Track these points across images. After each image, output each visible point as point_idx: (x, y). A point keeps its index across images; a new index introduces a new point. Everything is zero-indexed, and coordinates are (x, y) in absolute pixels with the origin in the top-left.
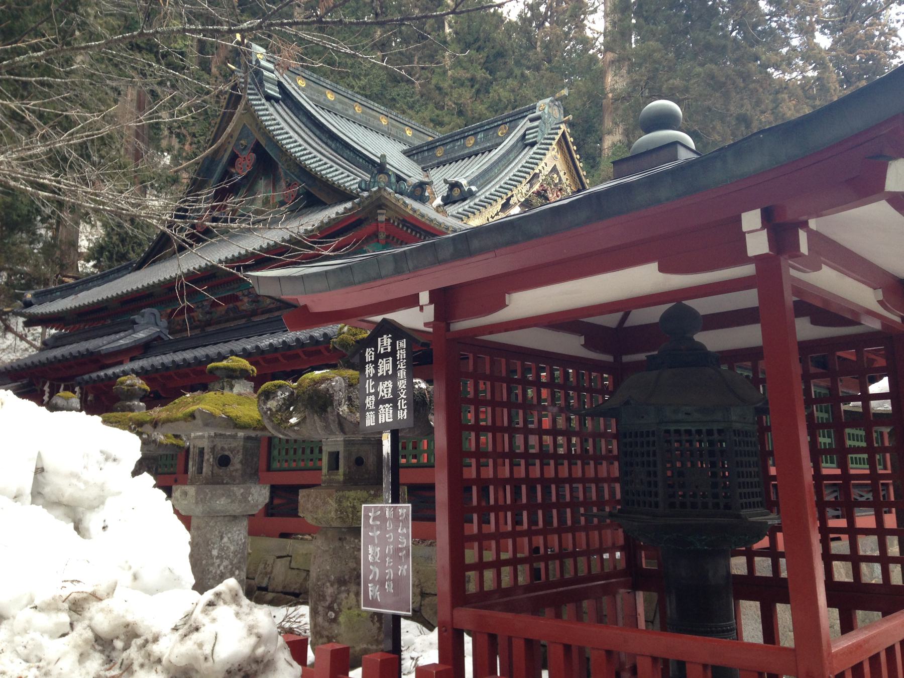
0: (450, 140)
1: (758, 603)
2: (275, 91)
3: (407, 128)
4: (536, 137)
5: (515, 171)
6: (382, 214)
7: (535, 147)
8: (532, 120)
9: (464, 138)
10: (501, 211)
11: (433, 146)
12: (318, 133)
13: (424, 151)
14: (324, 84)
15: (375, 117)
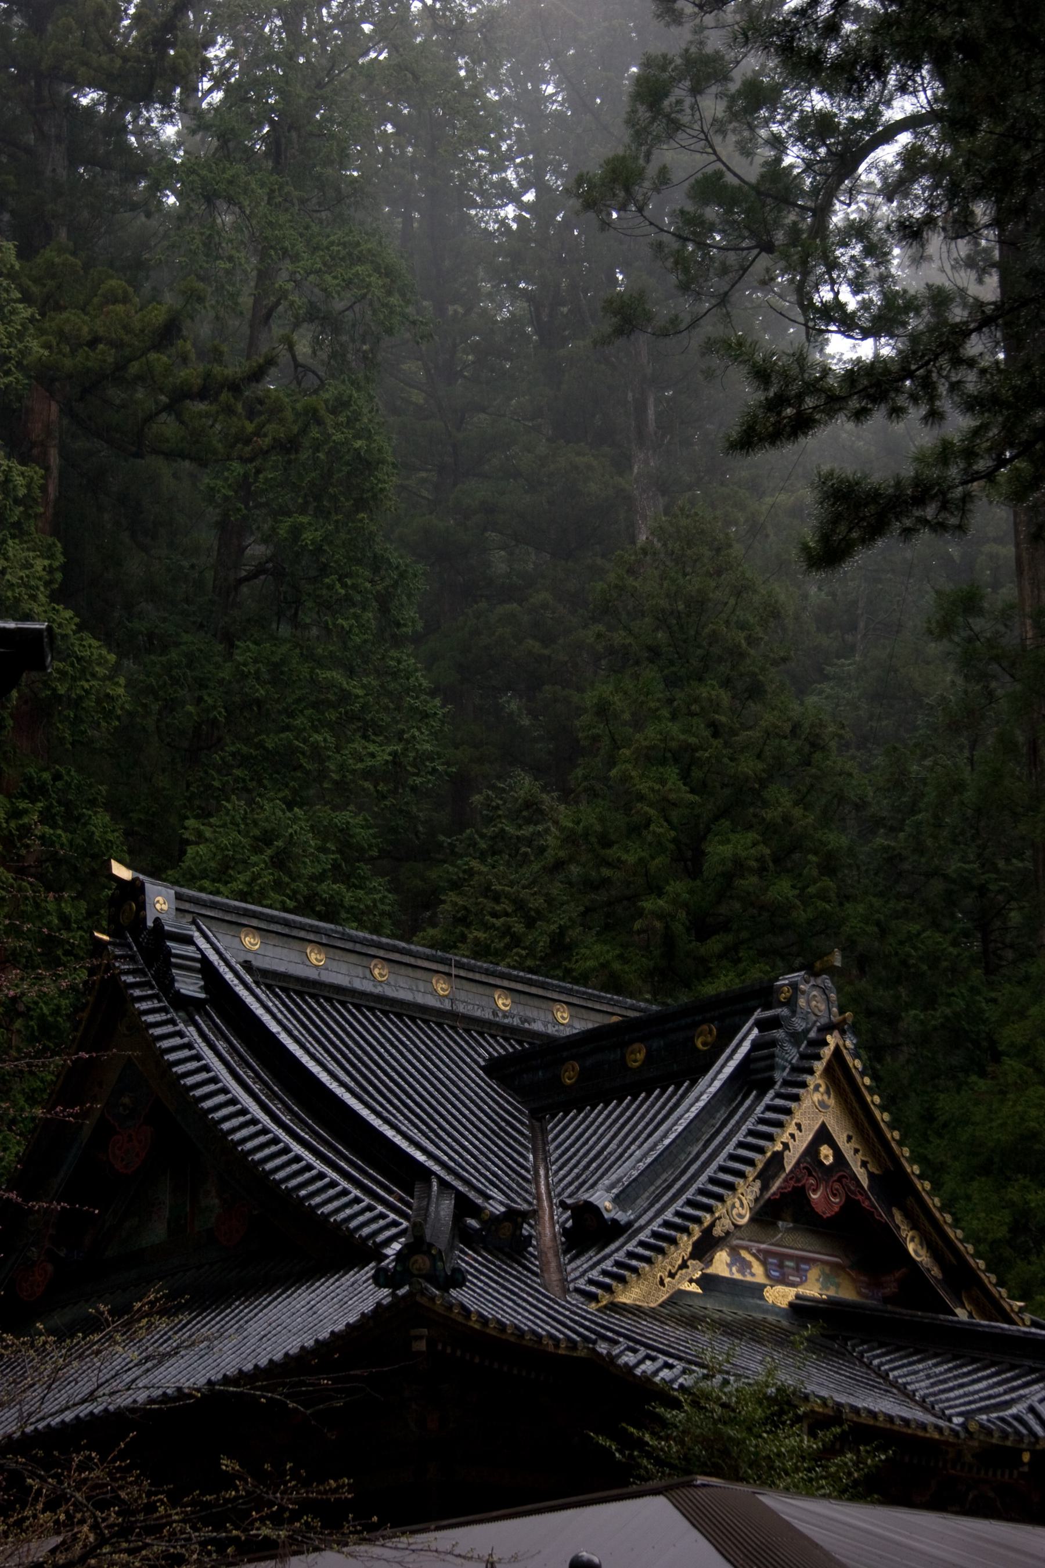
5: (702, 1181)
10: (693, 1256)
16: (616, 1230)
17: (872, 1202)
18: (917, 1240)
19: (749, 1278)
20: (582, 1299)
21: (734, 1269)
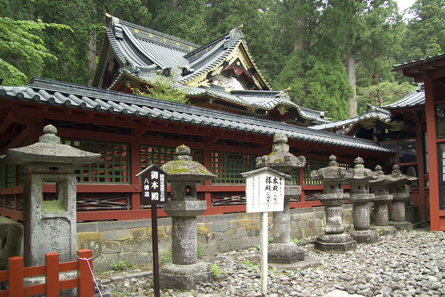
2: (121, 36)
4: (227, 46)
6: (128, 83)
7: (227, 50)
8: (227, 39)
9: (205, 48)
12: (135, 51)
14: (148, 31)
15: (173, 43)
16: (190, 73)
17: (248, 73)
19: (222, 86)
20: (251, 121)
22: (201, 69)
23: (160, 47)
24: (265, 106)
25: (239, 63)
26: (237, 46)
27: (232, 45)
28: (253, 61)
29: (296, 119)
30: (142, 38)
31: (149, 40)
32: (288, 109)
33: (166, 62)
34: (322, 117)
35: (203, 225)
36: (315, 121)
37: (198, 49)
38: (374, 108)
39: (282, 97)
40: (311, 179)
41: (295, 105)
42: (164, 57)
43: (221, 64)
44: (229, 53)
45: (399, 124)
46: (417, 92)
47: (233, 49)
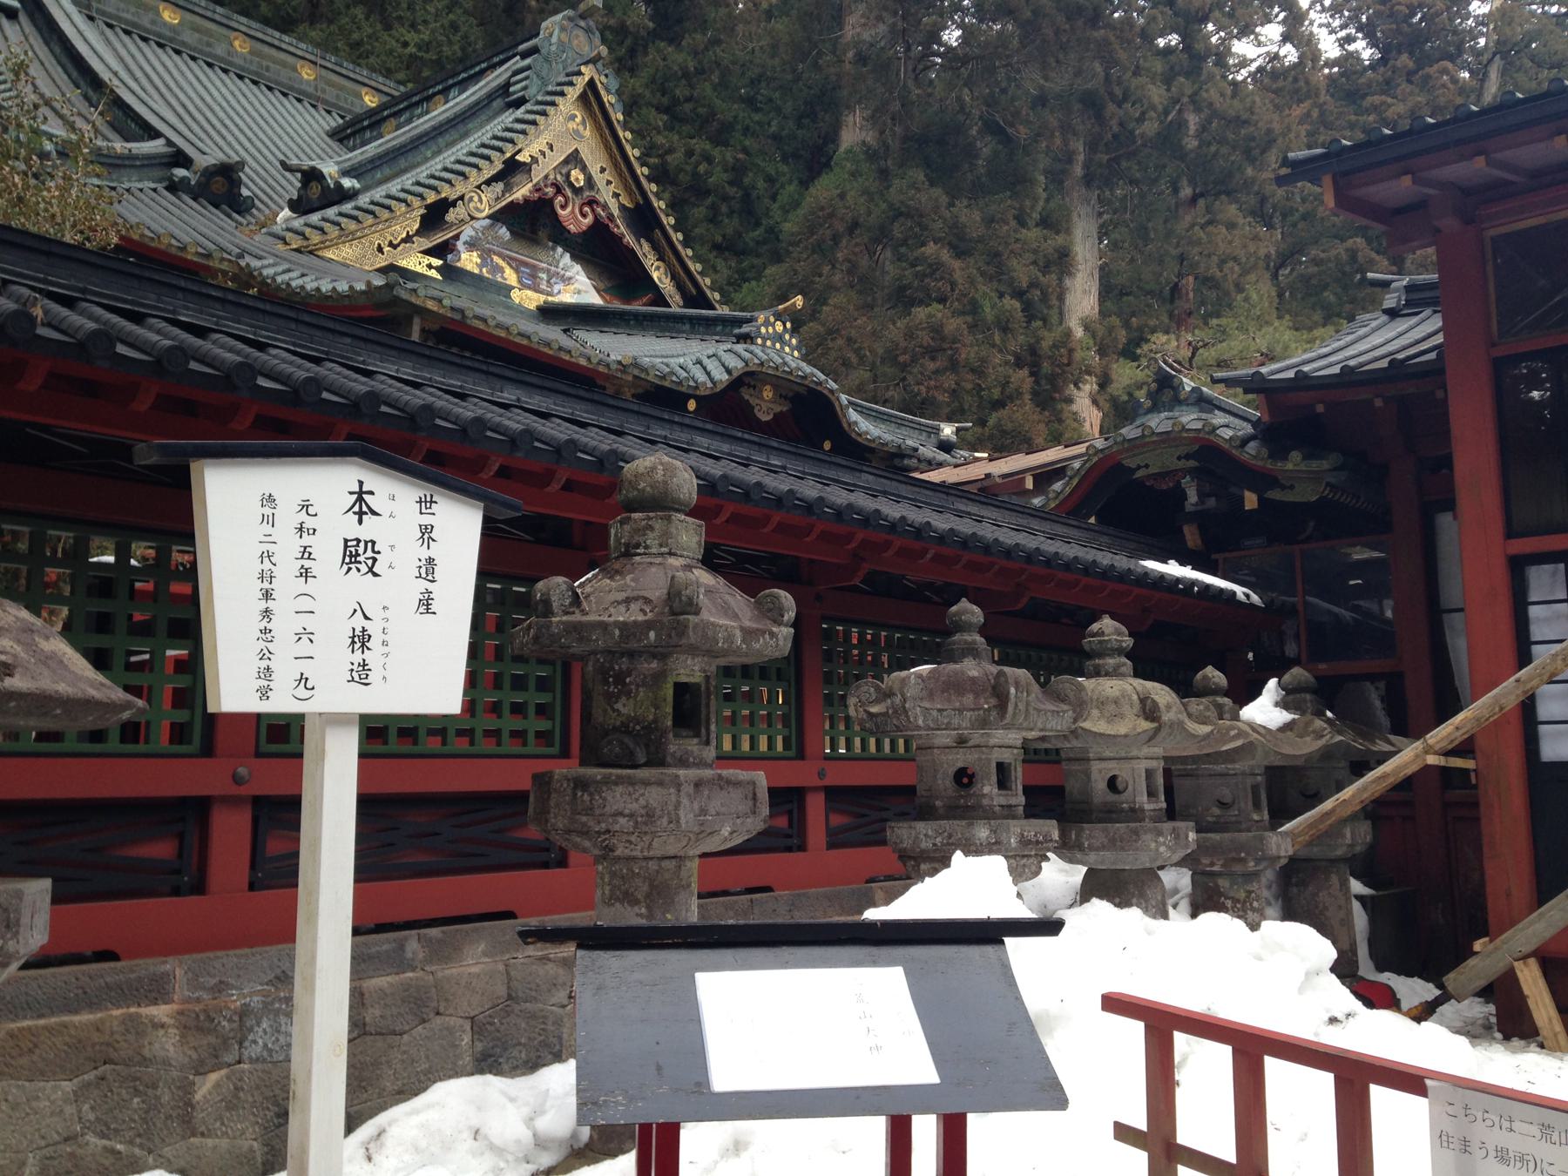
0: (405, 104)
1: (1331, 1076)
3: (364, 90)
4: (525, 88)
7: (522, 109)
8: (524, 55)
11: (378, 117)
12: (75, 74)
13: (364, 129)
15: (284, 64)
16: (344, 196)
18: (662, 270)
21: (484, 270)
22: (394, 187)
23: (215, 76)
24: (685, 375)
25: (581, 177)
26: (573, 93)
27: (550, 88)
28: (637, 152)
29: (827, 445)
30: (119, 19)
31: (159, 35)
32: (791, 394)
33: (234, 143)
34: (946, 447)
35: (165, 1019)
36: (911, 457)
37: (395, 100)
38: (1188, 384)
39: (764, 339)
40: (847, 727)
41: (822, 377)
42: (228, 122)
43: (493, 172)
44: (534, 123)
45: (1315, 465)
46: (1385, 318)
47: (553, 104)
